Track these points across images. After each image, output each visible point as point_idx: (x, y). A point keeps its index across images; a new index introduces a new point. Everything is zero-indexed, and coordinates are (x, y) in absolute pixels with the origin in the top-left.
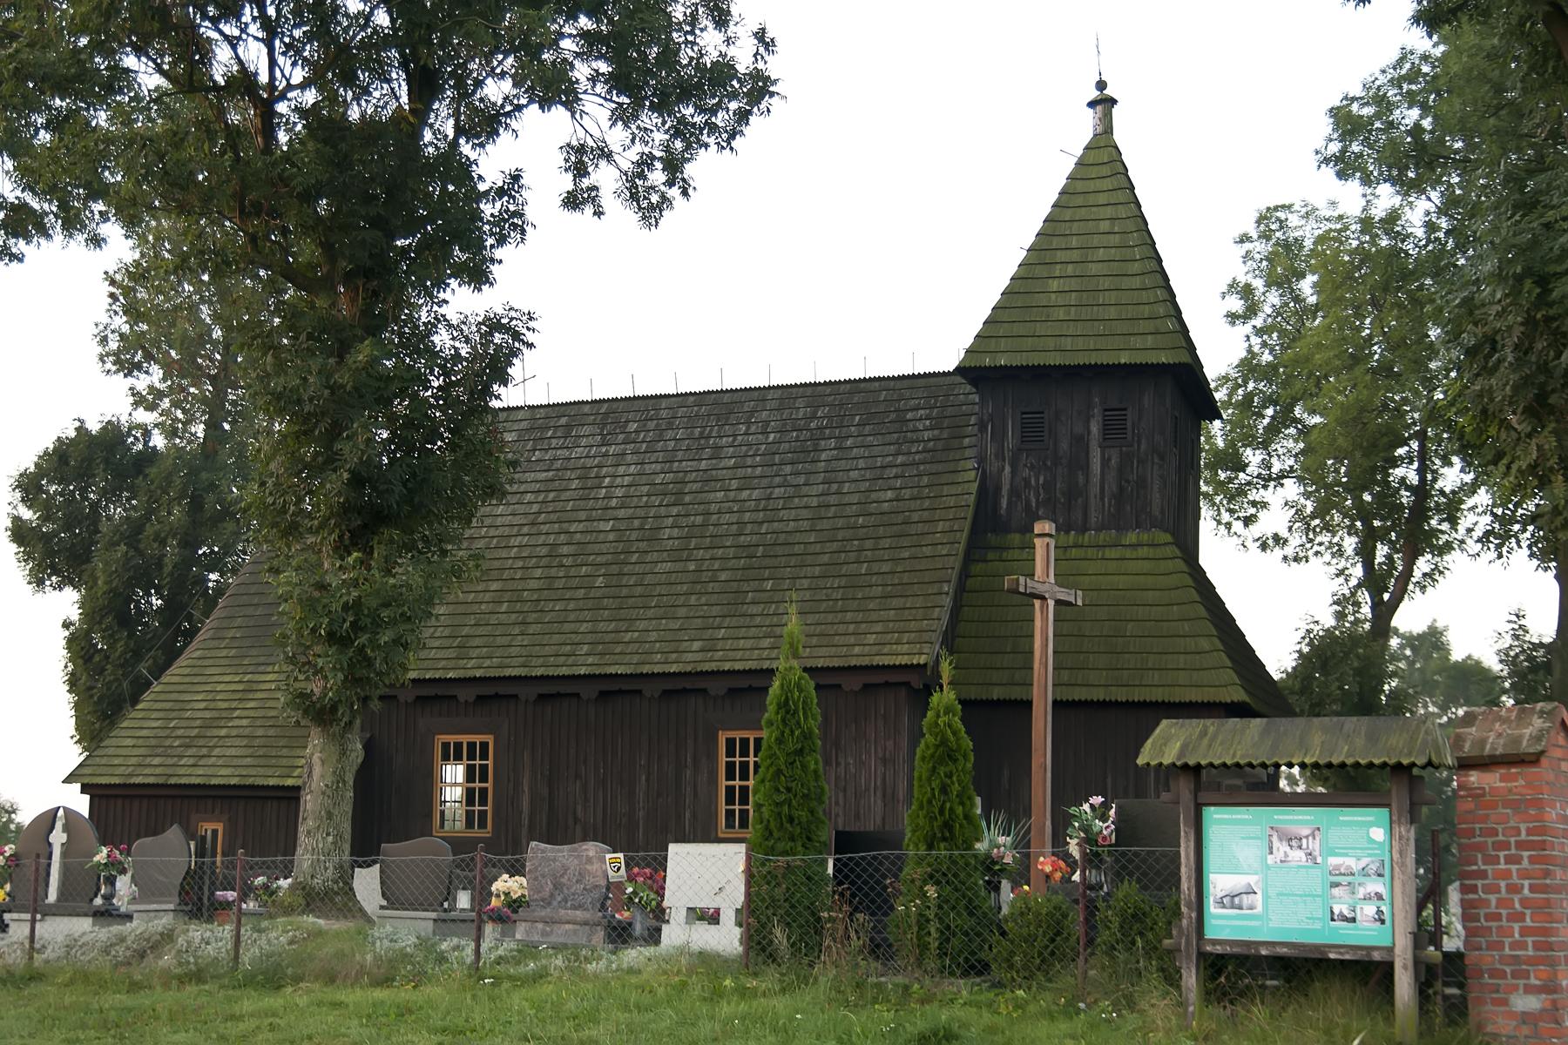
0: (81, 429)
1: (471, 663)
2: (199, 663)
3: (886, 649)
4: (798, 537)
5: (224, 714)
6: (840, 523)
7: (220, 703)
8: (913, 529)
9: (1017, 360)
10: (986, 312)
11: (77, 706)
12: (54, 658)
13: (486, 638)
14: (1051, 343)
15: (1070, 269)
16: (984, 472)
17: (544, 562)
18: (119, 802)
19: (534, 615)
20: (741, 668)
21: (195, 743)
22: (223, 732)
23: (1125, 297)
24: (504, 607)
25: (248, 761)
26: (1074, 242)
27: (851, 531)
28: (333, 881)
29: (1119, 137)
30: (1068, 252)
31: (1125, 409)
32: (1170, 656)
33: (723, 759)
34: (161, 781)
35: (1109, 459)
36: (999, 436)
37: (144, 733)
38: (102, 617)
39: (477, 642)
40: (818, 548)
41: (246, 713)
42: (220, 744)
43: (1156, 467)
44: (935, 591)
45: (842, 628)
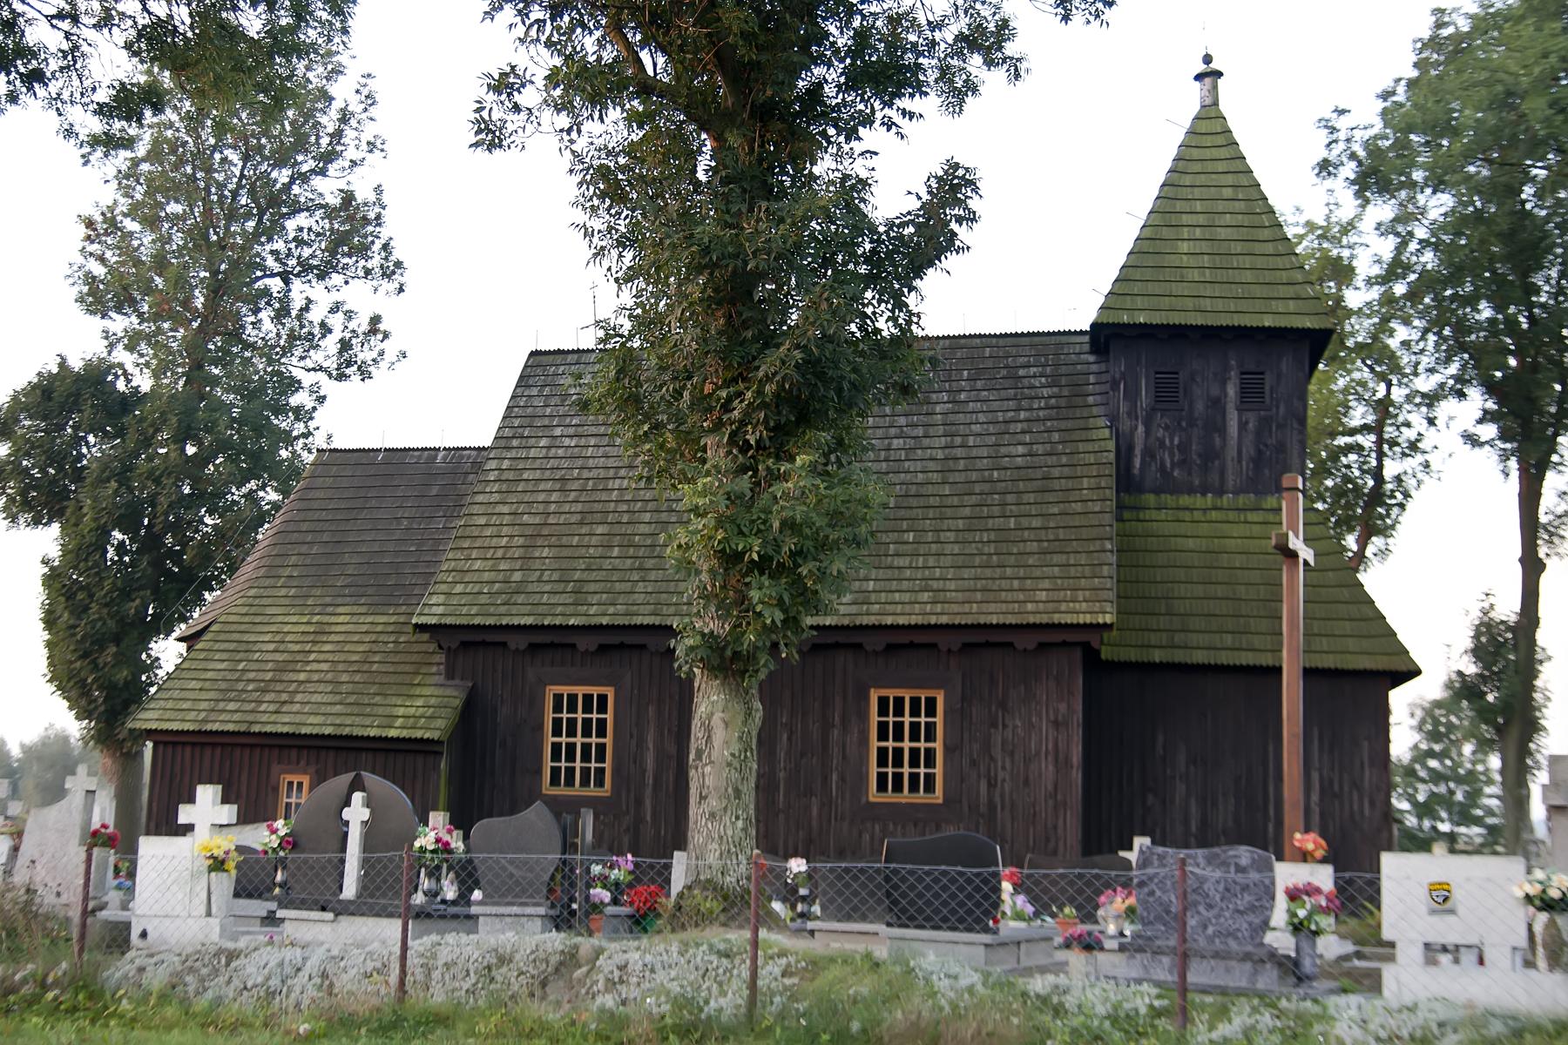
0: (63, 364)
1: (593, 610)
2: (257, 601)
3: (1063, 607)
4: (930, 489)
5: (299, 657)
6: (974, 476)
7: (290, 645)
8: (1056, 485)
9: (1157, 319)
11: (50, 645)
12: (34, 596)
13: (603, 584)
14: (1189, 303)
15: (1198, 233)
16: (1117, 430)
17: (650, 506)
18: (188, 750)
19: (653, 561)
20: (907, 623)
22: (302, 677)
23: (1260, 262)
24: (616, 552)
25: (338, 708)
26: (1198, 206)
27: (988, 485)
28: (748, 878)
29: (1224, 107)
30: (1194, 216)
31: (1262, 373)
32: (1334, 623)
33: (875, 718)
34: (243, 728)
36: (1132, 395)
37: (210, 675)
38: (89, 554)
39: (592, 587)
40: (955, 501)
41: (322, 657)
42: (301, 689)
43: (1295, 432)
44: (1098, 548)
45: (1005, 584)
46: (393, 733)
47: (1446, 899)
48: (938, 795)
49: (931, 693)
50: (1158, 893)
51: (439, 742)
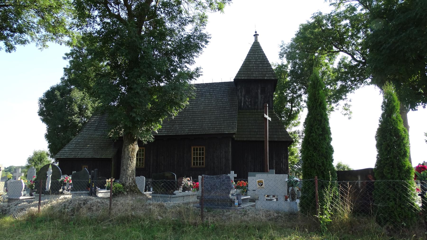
6: (212, 107)
10: (238, 70)
21: (82, 150)
33: (193, 152)
35: (262, 97)
36: (241, 92)
46: (103, 157)
47: (262, 185)
48: (204, 166)
49: (203, 147)
50: (206, 186)
51: (111, 159)
